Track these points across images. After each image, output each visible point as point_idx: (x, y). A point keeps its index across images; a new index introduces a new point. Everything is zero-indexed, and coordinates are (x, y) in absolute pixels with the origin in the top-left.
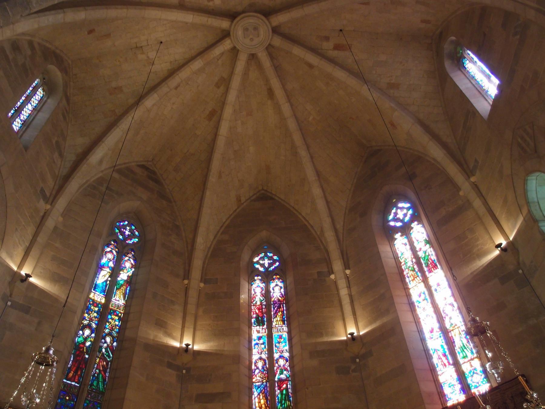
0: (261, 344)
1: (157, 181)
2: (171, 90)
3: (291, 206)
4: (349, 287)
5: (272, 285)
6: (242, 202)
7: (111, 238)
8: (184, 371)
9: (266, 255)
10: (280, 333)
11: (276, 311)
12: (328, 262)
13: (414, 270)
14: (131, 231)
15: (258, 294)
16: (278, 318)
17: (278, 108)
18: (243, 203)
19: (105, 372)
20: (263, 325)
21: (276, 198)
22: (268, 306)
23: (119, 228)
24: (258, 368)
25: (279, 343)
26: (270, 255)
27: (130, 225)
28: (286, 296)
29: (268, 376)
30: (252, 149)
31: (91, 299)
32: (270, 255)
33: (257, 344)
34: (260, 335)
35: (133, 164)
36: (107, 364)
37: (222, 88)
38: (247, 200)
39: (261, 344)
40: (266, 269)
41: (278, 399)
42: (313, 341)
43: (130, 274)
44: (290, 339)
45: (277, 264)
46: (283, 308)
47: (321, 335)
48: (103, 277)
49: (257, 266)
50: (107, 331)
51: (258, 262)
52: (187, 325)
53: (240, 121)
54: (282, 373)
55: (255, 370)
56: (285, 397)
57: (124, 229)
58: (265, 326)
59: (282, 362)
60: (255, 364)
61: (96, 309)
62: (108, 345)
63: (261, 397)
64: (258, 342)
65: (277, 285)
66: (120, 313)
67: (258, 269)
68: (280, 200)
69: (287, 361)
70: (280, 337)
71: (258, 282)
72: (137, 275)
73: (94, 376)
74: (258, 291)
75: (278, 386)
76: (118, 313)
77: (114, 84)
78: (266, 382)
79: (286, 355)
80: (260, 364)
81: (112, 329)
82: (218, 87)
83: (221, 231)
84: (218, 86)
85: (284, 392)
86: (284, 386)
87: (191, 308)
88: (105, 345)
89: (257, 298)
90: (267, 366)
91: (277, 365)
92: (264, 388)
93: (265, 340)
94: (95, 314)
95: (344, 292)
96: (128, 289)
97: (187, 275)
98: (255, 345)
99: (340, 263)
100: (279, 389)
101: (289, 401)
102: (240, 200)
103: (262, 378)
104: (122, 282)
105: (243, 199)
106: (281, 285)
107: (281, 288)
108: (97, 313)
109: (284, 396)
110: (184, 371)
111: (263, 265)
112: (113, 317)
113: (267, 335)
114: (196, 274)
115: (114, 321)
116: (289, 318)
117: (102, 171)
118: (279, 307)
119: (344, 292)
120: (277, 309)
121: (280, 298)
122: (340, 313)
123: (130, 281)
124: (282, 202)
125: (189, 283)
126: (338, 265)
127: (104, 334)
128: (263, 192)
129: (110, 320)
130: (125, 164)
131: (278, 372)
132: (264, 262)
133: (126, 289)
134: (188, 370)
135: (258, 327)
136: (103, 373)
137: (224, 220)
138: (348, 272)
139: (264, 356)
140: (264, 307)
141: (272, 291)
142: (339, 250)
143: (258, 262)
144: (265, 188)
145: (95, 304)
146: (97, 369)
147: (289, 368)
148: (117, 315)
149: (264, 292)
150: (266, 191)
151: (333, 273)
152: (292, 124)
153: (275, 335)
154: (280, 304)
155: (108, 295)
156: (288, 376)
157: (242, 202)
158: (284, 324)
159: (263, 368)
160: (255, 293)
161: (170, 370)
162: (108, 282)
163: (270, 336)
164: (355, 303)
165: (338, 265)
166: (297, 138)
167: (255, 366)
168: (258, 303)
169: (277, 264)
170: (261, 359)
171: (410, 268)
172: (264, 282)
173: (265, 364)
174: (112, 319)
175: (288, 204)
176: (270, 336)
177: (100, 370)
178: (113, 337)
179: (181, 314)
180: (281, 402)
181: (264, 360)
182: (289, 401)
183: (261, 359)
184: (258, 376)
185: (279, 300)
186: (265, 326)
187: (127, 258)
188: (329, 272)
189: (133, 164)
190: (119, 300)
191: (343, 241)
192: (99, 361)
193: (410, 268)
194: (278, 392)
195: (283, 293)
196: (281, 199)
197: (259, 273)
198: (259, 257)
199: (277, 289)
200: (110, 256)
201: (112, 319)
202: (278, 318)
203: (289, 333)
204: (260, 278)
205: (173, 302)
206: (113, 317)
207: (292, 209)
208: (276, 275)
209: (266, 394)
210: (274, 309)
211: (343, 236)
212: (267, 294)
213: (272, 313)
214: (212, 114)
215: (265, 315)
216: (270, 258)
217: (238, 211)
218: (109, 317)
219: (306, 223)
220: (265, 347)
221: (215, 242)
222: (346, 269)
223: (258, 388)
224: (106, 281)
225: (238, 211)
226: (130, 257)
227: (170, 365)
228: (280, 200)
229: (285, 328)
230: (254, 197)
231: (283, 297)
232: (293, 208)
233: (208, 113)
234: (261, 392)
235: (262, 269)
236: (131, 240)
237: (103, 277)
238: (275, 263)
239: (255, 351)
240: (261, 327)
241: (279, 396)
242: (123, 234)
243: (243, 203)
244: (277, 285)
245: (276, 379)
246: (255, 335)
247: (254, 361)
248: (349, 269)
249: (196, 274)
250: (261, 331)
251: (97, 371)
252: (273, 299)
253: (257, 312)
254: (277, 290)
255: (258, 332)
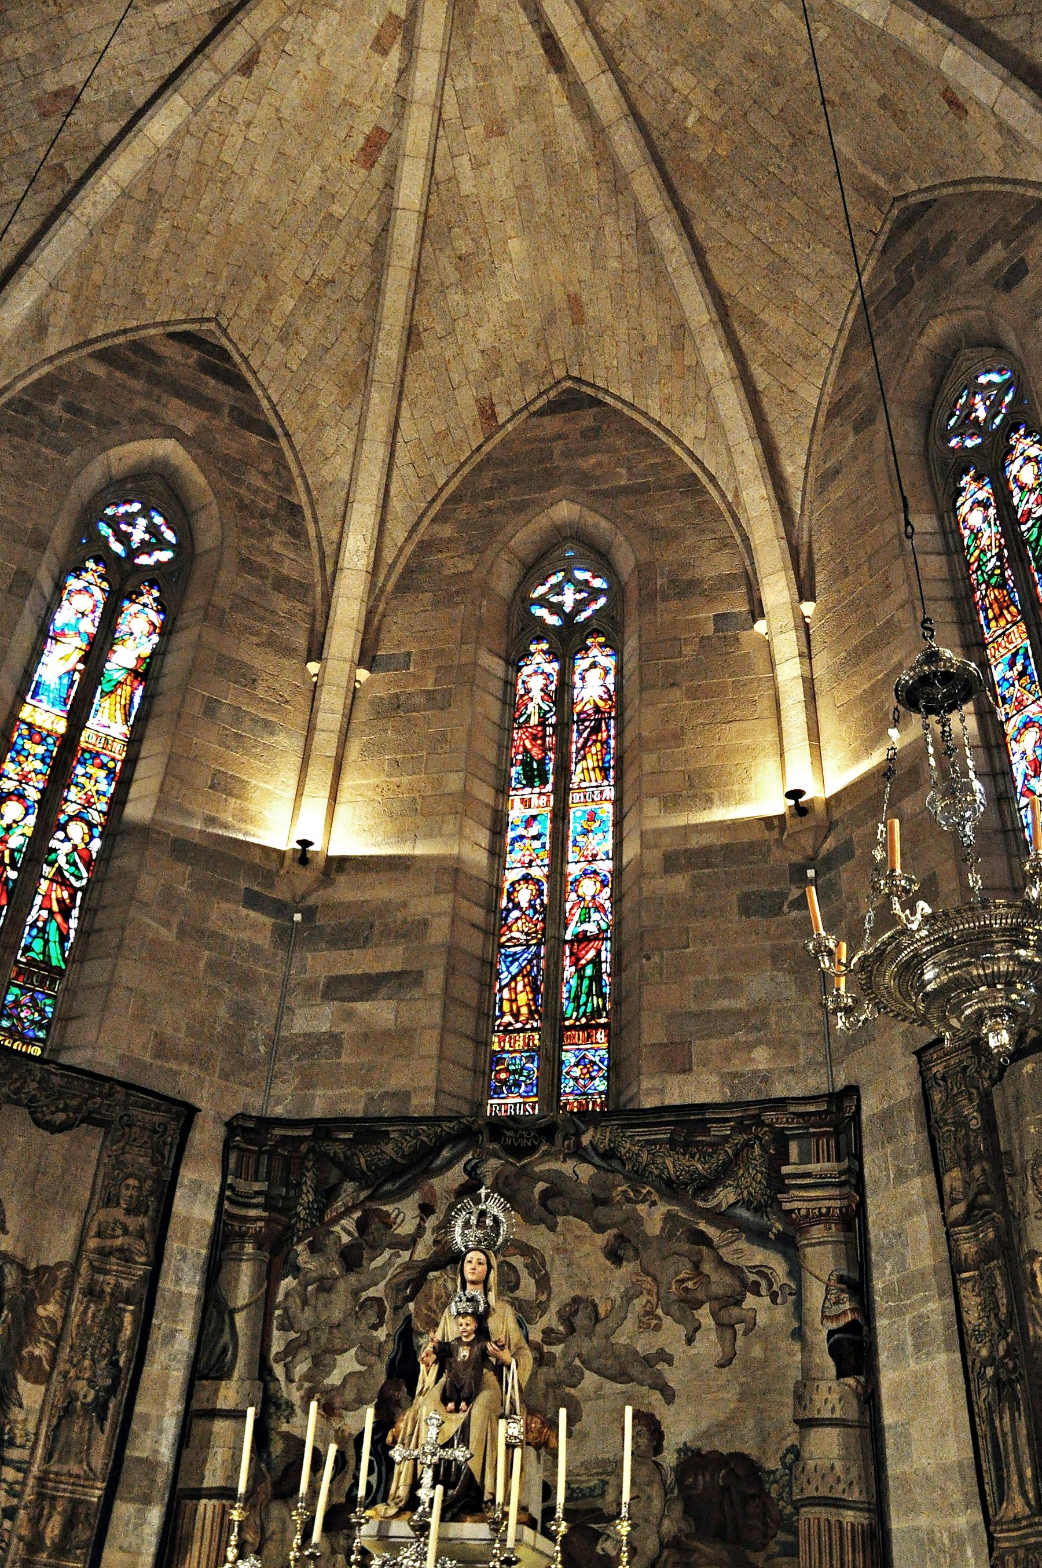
0: (534, 838)
1: (235, 380)
2: (225, 77)
3: (652, 420)
4: (807, 655)
5: (581, 664)
6: (501, 420)
7: (84, 549)
8: (298, 917)
9: (569, 579)
10: (592, 807)
11: (587, 740)
12: (751, 585)
13: (1002, 585)
14: (152, 529)
15: (537, 694)
16: (591, 762)
17: (576, 92)
18: (503, 425)
19: (66, 919)
20: (544, 782)
21: (609, 400)
22: (562, 729)
23: (113, 522)
24: (517, 906)
25: (586, 832)
26: (581, 575)
27: (144, 513)
28: (618, 697)
29: (544, 929)
30: (515, 246)
31: (23, 722)
32: (581, 575)
33: (522, 837)
34: (534, 812)
35: (153, 331)
36: (73, 897)
37: (395, 52)
38: (515, 414)
39: (534, 838)
40: (568, 618)
41: (570, 992)
42: (679, 820)
43: (146, 651)
44: (618, 823)
45: (602, 601)
46: (608, 730)
47: (708, 801)
48: (59, 663)
49: (539, 612)
50: (71, 809)
51: (542, 601)
52: (309, 787)
53: (466, 157)
54: (586, 919)
55: (509, 911)
56: (590, 987)
57: (129, 524)
58: (549, 787)
59: (588, 888)
60: (509, 894)
61: (40, 750)
62: (75, 848)
63: (520, 988)
64: (523, 832)
65: (594, 665)
66: (113, 759)
67: (541, 619)
68: (619, 406)
69: (604, 885)
70: (592, 817)
71: (539, 658)
72: (164, 654)
73: (33, 925)
74: (536, 684)
75: (572, 954)
76: (105, 759)
77: (50, 83)
78: (538, 945)
79: (605, 866)
80: (524, 895)
81: (88, 804)
82: (385, 53)
83: (431, 514)
84: (380, 46)
85: (589, 971)
86: (592, 953)
87: (326, 742)
88: (67, 847)
89: (531, 706)
90: (546, 900)
91: (573, 896)
92: (530, 962)
93: (542, 826)
94: (38, 765)
95: (789, 672)
96: (139, 693)
97: (316, 651)
98: (514, 840)
99: (783, 583)
100: (575, 963)
101: (601, 994)
102: (494, 416)
103: (527, 934)
104: (120, 676)
105: (503, 413)
106: (610, 662)
107: (606, 672)
108: (43, 761)
109: (586, 982)
110: (298, 917)
111: (556, 609)
112: (91, 770)
113: (554, 812)
114: (343, 639)
115: (92, 784)
116: (619, 768)
117: (51, 359)
118: (596, 730)
119: (789, 672)
120: (589, 735)
121: (601, 704)
122: (772, 737)
123: (146, 673)
124: (626, 410)
125: (323, 669)
126: (776, 590)
127: (63, 818)
128: (569, 384)
129: (82, 780)
130: (125, 331)
131: (576, 918)
132: (560, 598)
133: (132, 693)
134: (310, 914)
135: (528, 790)
136: (59, 918)
137: (441, 482)
138: (808, 608)
139: (536, 872)
140: (549, 730)
141: (579, 684)
142: (784, 543)
143: (542, 601)
144: (575, 373)
145: (37, 738)
146: (41, 908)
147: (607, 905)
148: (103, 766)
149: (552, 687)
150: (579, 380)
151: (762, 615)
152: (626, 144)
153: (577, 815)
154: (598, 721)
155: (78, 712)
156: (604, 926)
157: (501, 420)
158: (606, 777)
159: (532, 906)
160: (528, 691)
161: (253, 914)
162: (77, 676)
163: (560, 816)
164: (820, 702)
165: (776, 590)
166: (645, 185)
167: (510, 900)
168: (534, 720)
169: (602, 601)
170: (527, 878)
171: (993, 581)
172: (556, 658)
173: (540, 893)
174: (89, 777)
175: (645, 414)
176: (560, 816)
177: (51, 913)
178: (91, 826)
179: (296, 761)
180: (577, 998)
181: (537, 882)
182: (601, 994)
183: (527, 878)
184: (514, 928)
185: (597, 709)
186: (549, 787)
187: (135, 608)
188: (752, 612)
189: (153, 331)
190: (108, 723)
191: (802, 514)
192: (50, 889)
193: (993, 581)
194: (569, 971)
195: (612, 688)
196: (624, 402)
197: (542, 632)
198: (548, 585)
199: (594, 676)
200: (83, 602)
201: (89, 777)
202: (591, 762)
203: (618, 802)
204: (545, 646)
205: (269, 727)
206: (91, 770)
207: (654, 429)
208: (597, 633)
209: (535, 978)
210: (580, 734)
211: (803, 500)
212: (562, 693)
213: (574, 748)
214: (377, 142)
215: (551, 755)
216: (582, 586)
217: (486, 449)
218: (80, 770)
219: (695, 468)
220: (543, 845)
221: (410, 548)
222: (802, 598)
223: (512, 963)
224: (70, 673)
225: (486, 449)
226: (145, 605)
227: (252, 900)
228: (619, 406)
229: (610, 793)
230: (540, 403)
231: (610, 698)
232: (659, 424)
233: (361, 141)
234: (520, 972)
235: (553, 620)
236: (150, 554)
237: (59, 663)
238: (596, 600)
239: (512, 858)
240: (537, 790)
241: (574, 982)
242: (124, 538)
243: (503, 425)
244: (594, 665)
245: (568, 936)
246: (516, 813)
247: (507, 885)
248: (813, 598)
249: (343, 639)
250: (535, 800)
251: (45, 914)
252: (578, 708)
253: (527, 743)
254: (592, 687)
255: (526, 803)
